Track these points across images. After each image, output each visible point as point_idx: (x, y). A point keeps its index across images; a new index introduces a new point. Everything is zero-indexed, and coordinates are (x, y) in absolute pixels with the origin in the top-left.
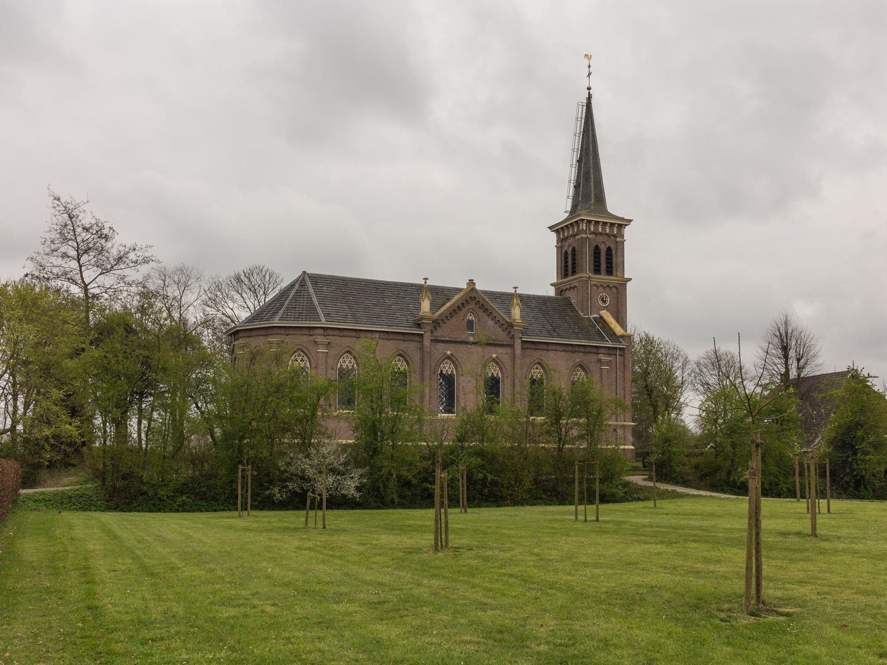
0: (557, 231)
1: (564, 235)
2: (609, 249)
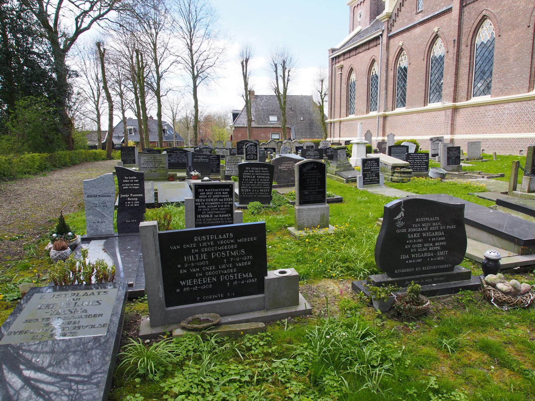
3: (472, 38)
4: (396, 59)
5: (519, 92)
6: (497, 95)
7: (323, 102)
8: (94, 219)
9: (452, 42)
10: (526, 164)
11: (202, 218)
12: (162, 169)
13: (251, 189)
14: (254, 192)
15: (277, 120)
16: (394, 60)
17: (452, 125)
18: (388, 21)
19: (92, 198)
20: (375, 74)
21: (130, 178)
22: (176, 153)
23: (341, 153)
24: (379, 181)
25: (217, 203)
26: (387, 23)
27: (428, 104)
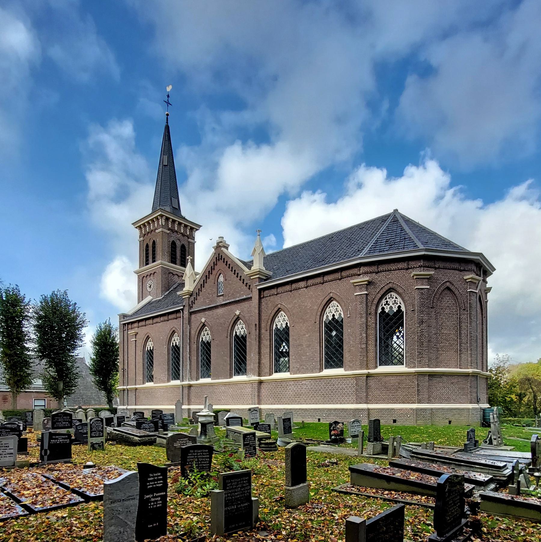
0: (140, 227)
1: (145, 230)
2: (183, 247)
3: (271, 325)
4: (199, 333)
5: (312, 372)
8: (116, 530)
9: (254, 326)
10: (369, 433)
12: (8, 456)
15: (42, 384)
16: (197, 334)
17: (259, 396)
18: (189, 298)
19: (115, 504)
20: (176, 345)
21: (154, 475)
26: (187, 299)
27: (234, 377)
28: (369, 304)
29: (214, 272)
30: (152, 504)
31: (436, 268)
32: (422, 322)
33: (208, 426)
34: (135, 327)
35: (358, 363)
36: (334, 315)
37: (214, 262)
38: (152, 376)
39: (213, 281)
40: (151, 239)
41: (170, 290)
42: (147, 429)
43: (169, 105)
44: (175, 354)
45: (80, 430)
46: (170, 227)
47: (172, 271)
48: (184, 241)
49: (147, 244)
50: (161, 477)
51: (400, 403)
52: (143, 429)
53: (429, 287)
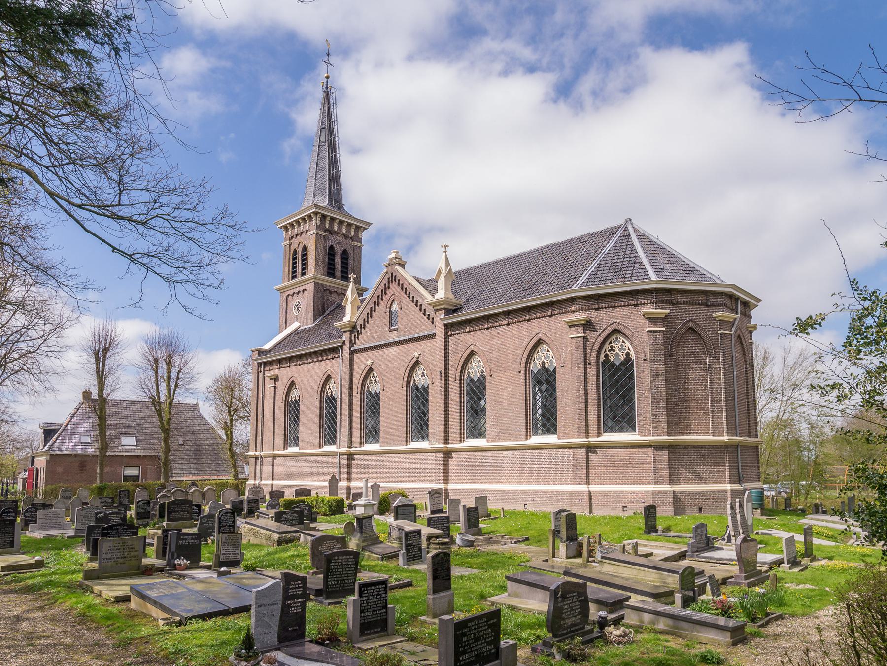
2: (345, 252)
4: (363, 380)
5: (516, 440)
6: (493, 440)
7: (231, 420)
11: (364, 616)
13: (337, 581)
14: (340, 584)
19: (262, 608)
21: (295, 583)
22: (117, 529)
23: (367, 524)
24: (421, 556)
25: (376, 600)
27: (412, 443)
28: (588, 350)
29: (386, 298)
30: (293, 609)
31: (673, 304)
32: (658, 375)
33: (364, 521)
34: (275, 369)
35: (575, 429)
36: (543, 363)
37: (385, 284)
38: (298, 438)
39: (384, 310)
40: (301, 244)
41: (326, 314)
42: (288, 520)
43: (330, 66)
44: (330, 408)
45: (206, 523)
46: (327, 226)
47: (328, 288)
48: (348, 245)
49: (295, 249)
50: (301, 585)
51: (631, 484)
52: (284, 521)
53: (664, 329)
